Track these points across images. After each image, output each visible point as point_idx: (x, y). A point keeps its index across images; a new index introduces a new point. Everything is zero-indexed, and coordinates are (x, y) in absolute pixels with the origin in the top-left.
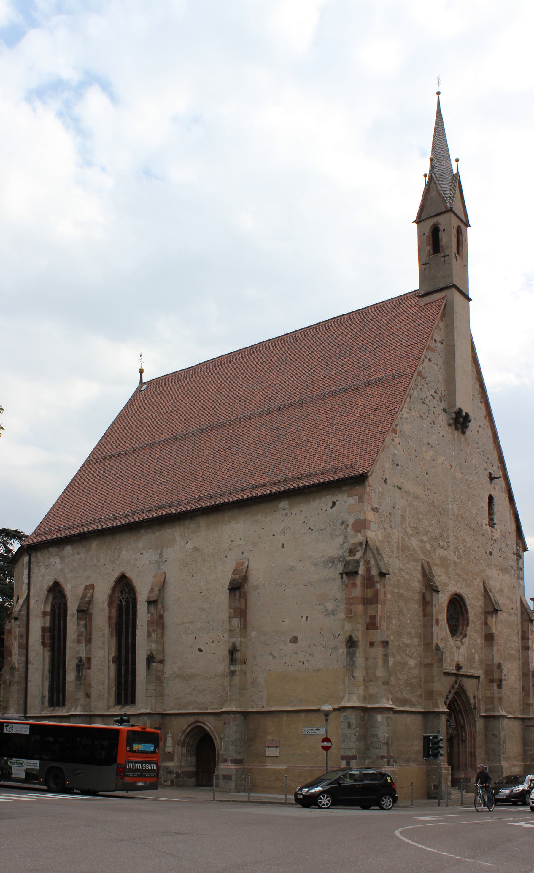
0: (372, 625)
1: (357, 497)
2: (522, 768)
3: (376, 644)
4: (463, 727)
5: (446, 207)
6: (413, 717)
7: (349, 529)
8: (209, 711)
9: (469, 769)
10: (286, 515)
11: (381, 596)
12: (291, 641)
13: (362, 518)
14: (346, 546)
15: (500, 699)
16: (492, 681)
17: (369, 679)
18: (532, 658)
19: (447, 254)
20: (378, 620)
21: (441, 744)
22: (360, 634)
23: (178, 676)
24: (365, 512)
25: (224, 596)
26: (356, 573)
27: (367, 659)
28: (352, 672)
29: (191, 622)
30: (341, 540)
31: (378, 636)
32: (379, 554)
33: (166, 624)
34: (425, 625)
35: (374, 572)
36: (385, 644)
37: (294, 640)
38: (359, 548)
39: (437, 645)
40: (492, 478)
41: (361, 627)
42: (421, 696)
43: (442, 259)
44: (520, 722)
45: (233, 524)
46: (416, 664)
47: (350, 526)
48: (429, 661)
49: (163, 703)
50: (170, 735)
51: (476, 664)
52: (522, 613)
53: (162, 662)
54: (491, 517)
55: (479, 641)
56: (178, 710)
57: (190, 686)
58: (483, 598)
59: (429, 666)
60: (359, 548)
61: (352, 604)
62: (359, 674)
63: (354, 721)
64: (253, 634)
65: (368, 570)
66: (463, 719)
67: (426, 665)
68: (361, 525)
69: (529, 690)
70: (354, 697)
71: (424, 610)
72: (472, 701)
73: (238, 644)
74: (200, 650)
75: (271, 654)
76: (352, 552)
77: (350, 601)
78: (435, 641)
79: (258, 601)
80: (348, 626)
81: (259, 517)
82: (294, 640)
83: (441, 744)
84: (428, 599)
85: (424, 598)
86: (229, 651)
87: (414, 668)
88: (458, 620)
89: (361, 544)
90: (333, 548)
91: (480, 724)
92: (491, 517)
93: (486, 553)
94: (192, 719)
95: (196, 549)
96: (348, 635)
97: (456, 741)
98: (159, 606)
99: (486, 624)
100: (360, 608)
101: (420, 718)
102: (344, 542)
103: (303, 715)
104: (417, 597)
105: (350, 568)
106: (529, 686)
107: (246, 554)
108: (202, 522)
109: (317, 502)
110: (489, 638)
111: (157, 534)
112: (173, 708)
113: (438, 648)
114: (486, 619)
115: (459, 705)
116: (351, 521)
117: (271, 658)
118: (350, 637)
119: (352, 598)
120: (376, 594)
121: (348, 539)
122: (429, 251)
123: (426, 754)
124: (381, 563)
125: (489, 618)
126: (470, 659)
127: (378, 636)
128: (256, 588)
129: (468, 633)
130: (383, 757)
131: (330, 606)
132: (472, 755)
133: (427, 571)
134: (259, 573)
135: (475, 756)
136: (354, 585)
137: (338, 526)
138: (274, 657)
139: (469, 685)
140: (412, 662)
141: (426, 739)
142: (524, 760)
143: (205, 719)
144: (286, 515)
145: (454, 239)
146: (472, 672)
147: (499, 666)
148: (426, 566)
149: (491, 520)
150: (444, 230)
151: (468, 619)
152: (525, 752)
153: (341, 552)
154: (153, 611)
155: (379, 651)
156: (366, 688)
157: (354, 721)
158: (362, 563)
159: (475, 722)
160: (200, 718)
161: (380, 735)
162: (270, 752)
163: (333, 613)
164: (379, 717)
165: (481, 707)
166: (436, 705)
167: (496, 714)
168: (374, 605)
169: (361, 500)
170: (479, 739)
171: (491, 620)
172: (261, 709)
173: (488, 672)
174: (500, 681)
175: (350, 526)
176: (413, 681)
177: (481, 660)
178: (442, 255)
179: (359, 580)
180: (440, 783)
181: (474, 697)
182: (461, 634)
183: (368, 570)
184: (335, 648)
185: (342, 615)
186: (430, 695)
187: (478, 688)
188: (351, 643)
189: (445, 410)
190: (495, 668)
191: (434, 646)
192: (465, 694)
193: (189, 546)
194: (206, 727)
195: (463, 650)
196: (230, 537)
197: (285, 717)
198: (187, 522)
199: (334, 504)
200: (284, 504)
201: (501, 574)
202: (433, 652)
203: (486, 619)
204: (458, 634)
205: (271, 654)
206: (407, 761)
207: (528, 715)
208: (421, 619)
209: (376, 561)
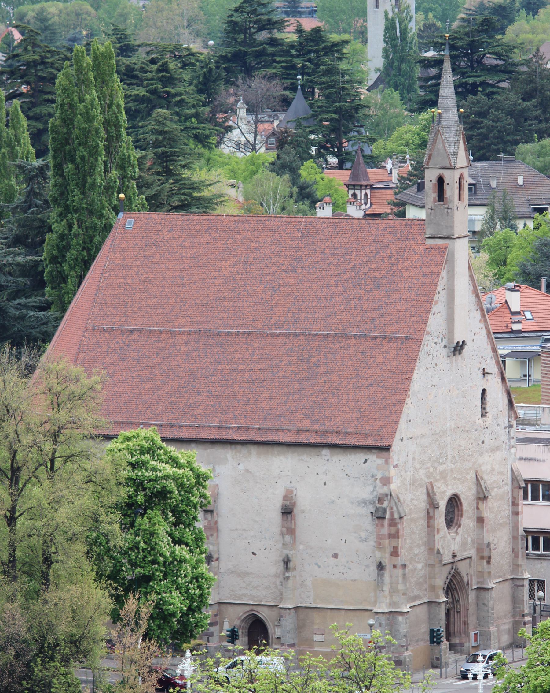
0: (395, 553)
1: (384, 460)
2: (511, 625)
3: (398, 567)
4: (458, 601)
5: (451, 165)
6: (421, 607)
7: (378, 482)
8: (263, 603)
9: (463, 635)
10: (328, 460)
11: (401, 532)
12: (332, 556)
13: (387, 476)
14: (375, 493)
15: (489, 573)
16: (482, 558)
17: (393, 591)
18: (521, 522)
19: (450, 207)
20: (399, 550)
21: (442, 639)
22: (387, 560)
23: (233, 572)
24: (389, 472)
25: (276, 516)
26: (384, 518)
27: (391, 576)
28: (382, 587)
29: (244, 530)
30: (371, 488)
31: (399, 561)
32: (399, 501)
33: (220, 527)
34: (429, 534)
35: (396, 516)
36: (404, 566)
37: (336, 556)
38: (386, 499)
39: (438, 549)
40: (484, 373)
41: (387, 555)
42: (426, 590)
43: (446, 210)
44: (510, 581)
45: (282, 458)
46: (423, 567)
47: (378, 480)
48: (432, 562)
49: (219, 594)
50: (226, 620)
51: (469, 546)
52: (513, 480)
53: (217, 560)
54: (484, 406)
55: (471, 525)
56: (234, 599)
57: (244, 582)
58: (475, 486)
59: (432, 566)
60: (386, 499)
61: (381, 539)
62: (386, 588)
63: (383, 622)
64: (301, 547)
65: (392, 514)
66: (458, 594)
67: (430, 565)
68: (386, 481)
69: (518, 552)
70: (384, 605)
71: (428, 522)
72: (465, 580)
73: (290, 556)
74: (254, 554)
75: (316, 564)
76: (380, 500)
77: (380, 537)
78: (436, 546)
79: (301, 520)
80: (378, 554)
81: (305, 457)
82: (336, 556)
83: (442, 639)
84: (431, 514)
85: (428, 513)
86: (284, 561)
87: (421, 570)
88: (454, 512)
89: (386, 495)
90: (366, 492)
91: (472, 596)
92: (484, 406)
93: (478, 444)
94: (248, 608)
95: (247, 471)
96: (378, 560)
97: (452, 612)
98: (215, 514)
99: (478, 508)
100: (387, 541)
101: (425, 606)
102: (374, 490)
103: (343, 612)
104: (423, 514)
105: (380, 514)
106: (518, 549)
107: (293, 484)
108: (254, 450)
109: (353, 456)
110: (480, 520)
111: (209, 451)
112: (229, 598)
113: (438, 552)
114: (478, 503)
115: (454, 586)
116: (379, 476)
117: (316, 567)
118: (380, 563)
119: (381, 535)
120: (398, 531)
121: (377, 488)
122: (434, 198)
123: (432, 642)
124: (400, 509)
125: (480, 503)
126: (464, 544)
127: (399, 561)
128: (303, 512)
129: (462, 523)
130: (403, 646)
131: (363, 535)
132: (466, 623)
133: (431, 492)
134: (304, 501)
135: (468, 624)
136: (383, 526)
137: (369, 477)
138: (319, 567)
139: (463, 567)
140: (420, 566)
141: (432, 631)
142: (513, 616)
143: (260, 609)
144: (328, 460)
145: (457, 191)
146: (466, 554)
147: (489, 545)
148: (430, 488)
149: (483, 408)
150: (448, 184)
151: (462, 511)
152: (514, 608)
153: (371, 497)
154: (209, 518)
155: (399, 572)
156: (391, 597)
157: (383, 622)
158: (388, 510)
159: (468, 596)
160: (254, 608)
161: (401, 630)
162: (316, 638)
163: (366, 540)
164: (400, 618)
165: (474, 581)
166: (438, 596)
167: (486, 586)
168: (396, 539)
169: (387, 462)
170: (472, 609)
171: (482, 506)
172: (309, 605)
173: (479, 550)
174: (490, 557)
175: (378, 480)
176: (421, 580)
177: (473, 541)
178: (446, 206)
179: (386, 522)
180: (441, 655)
181: (467, 575)
182: (457, 524)
183: (392, 514)
184: (367, 566)
185: (372, 543)
186: (433, 588)
187: (470, 566)
188: (381, 567)
189: (445, 347)
190: (485, 547)
191: (436, 550)
192: (460, 575)
193: (241, 467)
194: (260, 615)
195: (458, 539)
196: (279, 467)
197: (329, 613)
198: (233, 446)
199: (366, 461)
200: (325, 452)
201: (492, 455)
202: (433, 551)
203: (478, 503)
204: (454, 525)
205: (316, 564)
206: (417, 641)
207: (517, 575)
208: (426, 530)
209: (397, 508)
